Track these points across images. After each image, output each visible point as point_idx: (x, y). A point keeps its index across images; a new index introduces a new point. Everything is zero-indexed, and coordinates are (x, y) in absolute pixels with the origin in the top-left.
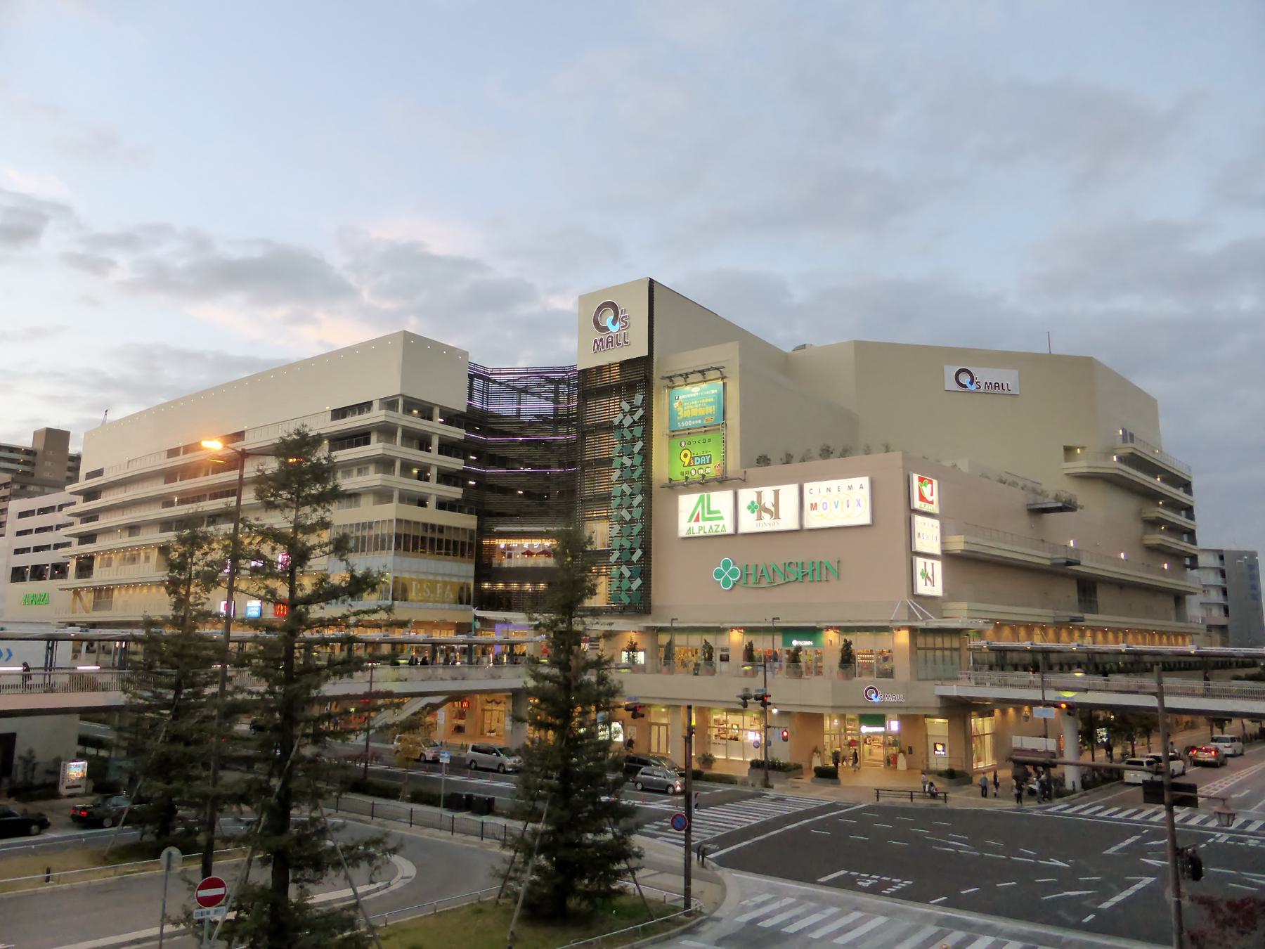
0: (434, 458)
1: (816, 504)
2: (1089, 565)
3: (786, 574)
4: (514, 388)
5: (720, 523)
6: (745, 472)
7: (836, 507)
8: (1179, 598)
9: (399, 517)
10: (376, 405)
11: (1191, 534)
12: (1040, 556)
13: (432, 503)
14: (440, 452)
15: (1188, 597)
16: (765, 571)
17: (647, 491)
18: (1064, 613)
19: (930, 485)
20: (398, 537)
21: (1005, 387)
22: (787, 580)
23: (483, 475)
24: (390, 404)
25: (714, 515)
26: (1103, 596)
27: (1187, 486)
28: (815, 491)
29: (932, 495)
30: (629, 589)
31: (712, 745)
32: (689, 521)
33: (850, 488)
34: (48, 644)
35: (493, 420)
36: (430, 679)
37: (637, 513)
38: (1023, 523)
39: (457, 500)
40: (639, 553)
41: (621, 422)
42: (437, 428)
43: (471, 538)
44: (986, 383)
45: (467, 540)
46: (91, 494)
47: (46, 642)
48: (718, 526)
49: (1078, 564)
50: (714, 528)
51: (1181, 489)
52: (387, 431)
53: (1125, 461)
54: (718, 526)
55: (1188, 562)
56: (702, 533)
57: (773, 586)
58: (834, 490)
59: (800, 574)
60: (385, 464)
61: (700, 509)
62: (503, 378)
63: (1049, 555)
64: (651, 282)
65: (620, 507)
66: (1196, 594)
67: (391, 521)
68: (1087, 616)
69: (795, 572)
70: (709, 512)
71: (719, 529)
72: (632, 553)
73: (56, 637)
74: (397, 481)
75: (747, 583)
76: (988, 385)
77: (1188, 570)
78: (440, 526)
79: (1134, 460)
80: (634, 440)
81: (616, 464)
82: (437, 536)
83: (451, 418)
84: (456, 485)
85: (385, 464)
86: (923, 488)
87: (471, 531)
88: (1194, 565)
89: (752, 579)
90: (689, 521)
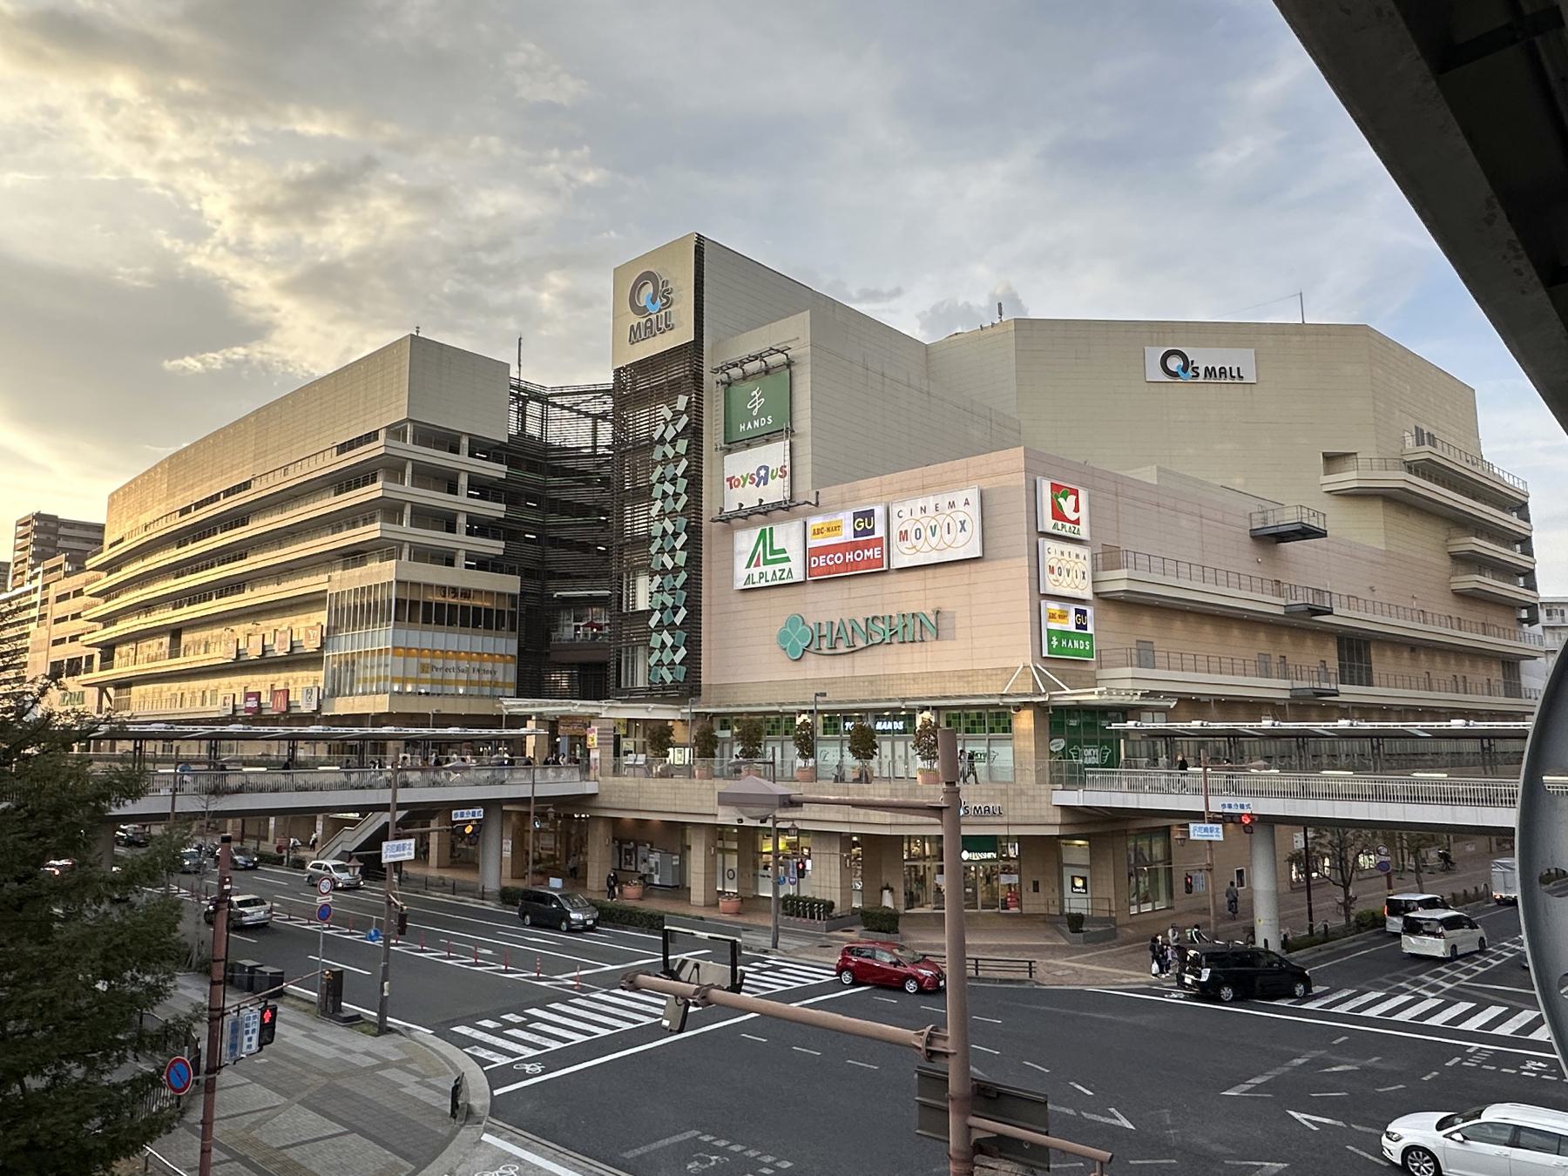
0: (463, 502)
1: (906, 531)
2: (1344, 615)
3: (868, 636)
4: (587, 415)
5: (785, 565)
6: (818, 493)
7: (934, 535)
8: (1510, 664)
9: (401, 578)
10: (382, 434)
11: (1529, 575)
12: (1271, 604)
13: (461, 560)
15: (1524, 664)
16: (842, 629)
17: (694, 532)
18: (1306, 684)
19: (1074, 497)
20: (400, 603)
21: (1235, 374)
22: (870, 642)
23: (543, 526)
24: (395, 431)
25: (780, 556)
26: (1382, 663)
27: (1521, 509)
28: (906, 514)
29: (1077, 510)
30: (672, 663)
31: (760, 878)
32: (748, 566)
34: (135, 744)
35: (554, 454)
36: (435, 784)
37: (681, 557)
38: (1246, 558)
40: (683, 613)
41: (662, 435)
42: (461, 461)
43: (514, 605)
44: (1207, 368)
45: (507, 608)
46: (111, 567)
47: (208, 742)
48: (784, 570)
49: (1330, 613)
50: (778, 574)
51: (1515, 514)
52: (391, 467)
53: (1417, 471)
54: (784, 570)
55: (1524, 614)
56: (763, 583)
57: (853, 651)
59: (888, 634)
60: (389, 510)
61: (760, 548)
62: (565, 401)
63: (1282, 601)
64: (700, 238)
65: (661, 551)
66: (1535, 658)
67: (390, 583)
68: (1342, 688)
70: (773, 552)
71: (785, 575)
72: (675, 614)
73: (1492, 734)
74: (405, 530)
75: (820, 649)
76: (1209, 372)
77: (1526, 625)
78: (463, 589)
80: (678, 457)
81: (657, 493)
82: (450, 600)
83: (482, 448)
84: (496, 537)
85: (389, 510)
86: (1061, 500)
87: (512, 596)
88: (1533, 620)
89: (825, 644)
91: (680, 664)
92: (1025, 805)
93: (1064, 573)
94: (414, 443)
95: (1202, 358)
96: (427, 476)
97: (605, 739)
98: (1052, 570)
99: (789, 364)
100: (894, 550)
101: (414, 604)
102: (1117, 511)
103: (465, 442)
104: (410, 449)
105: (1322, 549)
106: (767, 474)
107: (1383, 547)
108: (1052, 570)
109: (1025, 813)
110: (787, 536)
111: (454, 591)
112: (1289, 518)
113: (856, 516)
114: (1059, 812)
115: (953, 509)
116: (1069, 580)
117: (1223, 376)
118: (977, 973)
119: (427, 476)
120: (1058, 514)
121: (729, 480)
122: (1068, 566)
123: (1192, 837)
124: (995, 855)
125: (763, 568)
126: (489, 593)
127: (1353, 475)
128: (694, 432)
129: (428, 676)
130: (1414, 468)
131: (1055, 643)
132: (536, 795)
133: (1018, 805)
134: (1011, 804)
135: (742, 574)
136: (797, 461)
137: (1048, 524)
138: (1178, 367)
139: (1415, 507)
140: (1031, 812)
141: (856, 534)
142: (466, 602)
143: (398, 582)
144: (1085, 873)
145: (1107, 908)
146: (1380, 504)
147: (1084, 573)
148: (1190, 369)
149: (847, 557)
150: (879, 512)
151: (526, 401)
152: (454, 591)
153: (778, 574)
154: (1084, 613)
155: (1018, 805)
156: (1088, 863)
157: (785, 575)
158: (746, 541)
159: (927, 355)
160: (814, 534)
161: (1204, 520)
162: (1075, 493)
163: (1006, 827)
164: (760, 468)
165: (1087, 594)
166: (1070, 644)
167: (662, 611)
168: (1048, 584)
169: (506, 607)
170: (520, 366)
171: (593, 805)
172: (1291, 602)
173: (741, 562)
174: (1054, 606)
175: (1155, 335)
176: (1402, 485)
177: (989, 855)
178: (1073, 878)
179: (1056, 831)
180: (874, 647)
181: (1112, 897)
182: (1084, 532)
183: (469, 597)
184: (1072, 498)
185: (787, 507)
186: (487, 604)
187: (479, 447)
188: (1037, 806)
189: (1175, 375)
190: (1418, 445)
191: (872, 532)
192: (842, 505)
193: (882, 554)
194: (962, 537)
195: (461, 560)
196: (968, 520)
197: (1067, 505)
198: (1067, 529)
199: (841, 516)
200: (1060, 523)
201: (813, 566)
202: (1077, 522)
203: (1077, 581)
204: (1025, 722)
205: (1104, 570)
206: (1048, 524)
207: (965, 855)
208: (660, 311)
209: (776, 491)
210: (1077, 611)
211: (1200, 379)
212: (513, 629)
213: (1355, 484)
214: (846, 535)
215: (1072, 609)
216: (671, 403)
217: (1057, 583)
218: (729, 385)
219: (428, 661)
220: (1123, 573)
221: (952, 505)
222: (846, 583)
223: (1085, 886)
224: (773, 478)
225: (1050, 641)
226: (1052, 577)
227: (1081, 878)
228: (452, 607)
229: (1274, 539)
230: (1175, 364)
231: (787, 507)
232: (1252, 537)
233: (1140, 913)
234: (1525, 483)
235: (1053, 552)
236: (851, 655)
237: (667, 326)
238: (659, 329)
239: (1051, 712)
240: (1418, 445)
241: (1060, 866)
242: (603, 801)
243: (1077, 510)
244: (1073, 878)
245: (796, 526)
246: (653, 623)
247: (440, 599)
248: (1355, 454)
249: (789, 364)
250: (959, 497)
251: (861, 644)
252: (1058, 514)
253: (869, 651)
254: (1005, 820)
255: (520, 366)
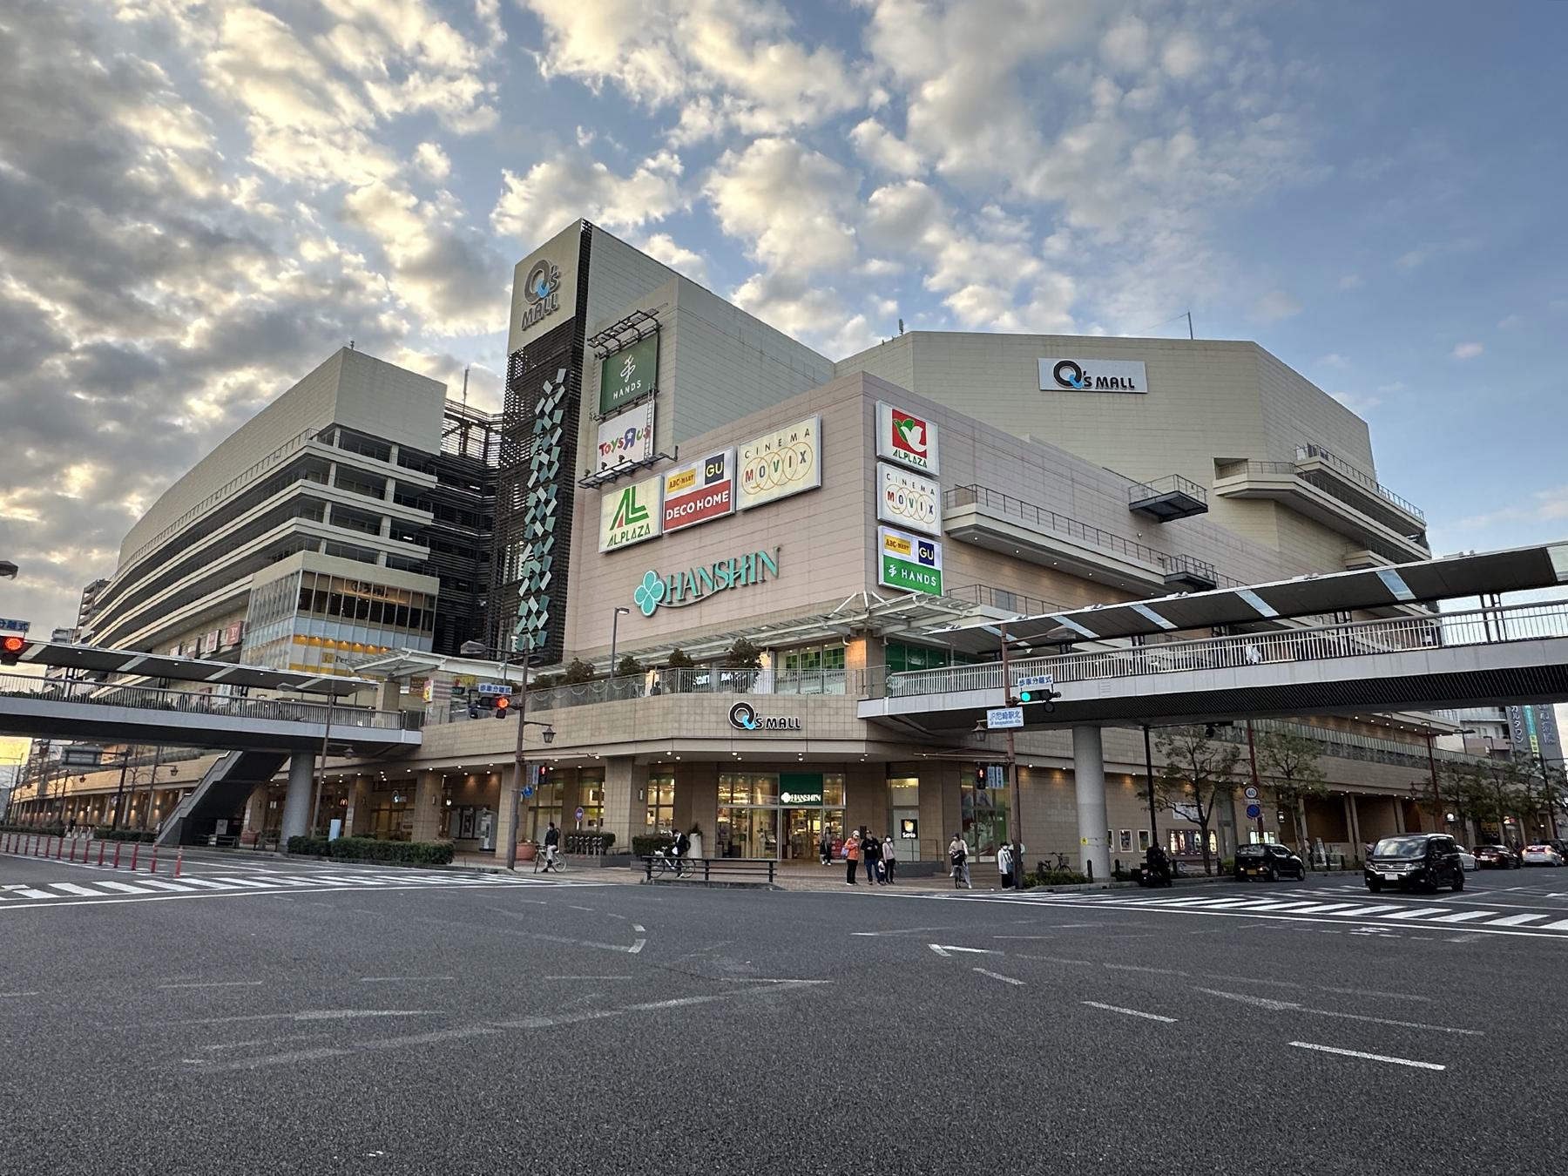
0: (387, 506)
6: (677, 448)
7: (776, 471)
13: (382, 559)
14: (397, 500)
16: (691, 579)
20: (306, 594)
27: (1421, 538)
29: (923, 442)
32: (612, 529)
33: (794, 438)
38: (1126, 527)
39: (423, 561)
42: (391, 469)
43: (431, 606)
44: (1099, 379)
50: (638, 531)
52: (313, 467)
56: (625, 543)
58: (774, 448)
69: (727, 575)
71: (643, 532)
76: (1102, 382)
79: (1321, 478)
82: (370, 596)
87: (431, 598)
90: (612, 529)
91: (542, 629)
92: (826, 719)
93: (906, 503)
94: (340, 447)
95: (1095, 369)
96: (350, 478)
97: (441, 693)
98: (891, 495)
99: (658, 329)
100: (740, 491)
101: (322, 596)
102: (974, 456)
103: (395, 451)
104: (336, 453)
105: (1210, 538)
106: (633, 437)
107: (1278, 550)
108: (891, 495)
109: (826, 727)
110: (648, 493)
111: (367, 586)
112: (1164, 488)
113: (708, 463)
114: (864, 726)
115: (795, 442)
116: (912, 511)
117: (1115, 386)
118: (707, 878)
119: (350, 478)
120: (900, 441)
121: (601, 447)
122: (911, 496)
123: (990, 727)
124: (819, 798)
125: (625, 528)
126: (416, 594)
127: (1244, 477)
128: (571, 405)
129: (331, 666)
130: (1307, 476)
131: (893, 572)
132: (330, 737)
133: (818, 719)
134: (810, 718)
135: (608, 536)
136: (661, 420)
137: (889, 450)
138: (1071, 377)
139: (1311, 519)
140: (834, 726)
141: (708, 481)
142: (379, 598)
143: (304, 572)
144: (913, 815)
145: (934, 851)
146: (1272, 507)
147: (931, 507)
148: (1082, 379)
149: (699, 505)
150: (728, 454)
151: (468, 425)
152: (367, 586)
153: (638, 531)
154: (931, 548)
155: (818, 719)
156: (916, 802)
157: (643, 532)
158: (612, 502)
159: (835, 373)
160: (671, 486)
161: (1076, 485)
162: (923, 425)
163: (805, 743)
164: (628, 432)
165: (935, 529)
166: (912, 576)
167: (530, 579)
168: (886, 508)
169: (422, 606)
170: (465, 394)
171: (416, 758)
172: (1170, 572)
173: (607, 522)
174: (894, 535)
175: (1049, 347)
176: (1292, 487)
177: (813, 798)
178: (903, 822)
179: (860, 749)
180: (720, 594)
181: (940, 838)
182: (931, 465)
183: (382, 595)
184: (918, 430)
185: (649, 465)
186: (403, 602)
187: (410, 458)
188: (841, 719)
189: (1068, 384)
190: (1310, 456)
191: (721, 476)
192: (697, 455)
193: (729, 498)
194: (801, 468)
195: (382, 559)
196: (808, 450)
197: (912, 437)
198: (912, 459)
199: (694, 465)
200: (902, 452)
201: (668, 518)
202: (924, 454)
203: (922, 514)
204: (857, 653)
205: (956, 506)
206: (889, 450)
207: (786, 797)
208: (548, 295)
209: (638, 453)
210: (921, 544)
211: (1093, 389)
212: (430, 630)
213: (1246, 486)
214: (699, 483)
215: (915, 540)
216: (552, 379)
217: (897, 511)
218: (608, 357)
219: (332, 651)
220: (972, 507)
221: (794, 438)
222: (697, 533)
223: (915, 831)
224: (639, 439)
225: (887, 569)
226: (890, 503)
227: (911, 821)
228: (363, 602)
229: (1156, 517)
230: (1067, 374)
231: (649, 465)
232: (1131, 511)
233: (978, 863)
234: (1421, 512)
235: (892, 479)
236: (698, 606)
237: (553, 306)
238: (546, 311)
239: (886, 643)
240: (1310, 456)
241: (890, 809)
242: (424, 753)
243: (923, 442)
244: (903, 822)
245: (655, 481)
246: (522, 592)
247: (351, 593)
248: (1246, 460)
249: (658, 329)
250: (800, 428)
251: (707, 593)
252: (900, 441)
253: (715, 599)
254: (803, 735)
255: (465, 394)
